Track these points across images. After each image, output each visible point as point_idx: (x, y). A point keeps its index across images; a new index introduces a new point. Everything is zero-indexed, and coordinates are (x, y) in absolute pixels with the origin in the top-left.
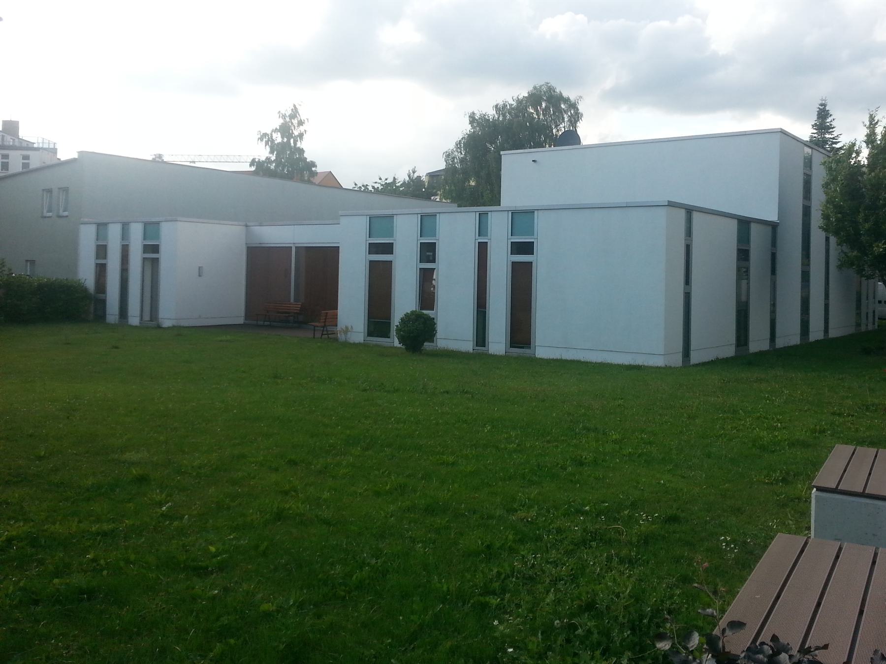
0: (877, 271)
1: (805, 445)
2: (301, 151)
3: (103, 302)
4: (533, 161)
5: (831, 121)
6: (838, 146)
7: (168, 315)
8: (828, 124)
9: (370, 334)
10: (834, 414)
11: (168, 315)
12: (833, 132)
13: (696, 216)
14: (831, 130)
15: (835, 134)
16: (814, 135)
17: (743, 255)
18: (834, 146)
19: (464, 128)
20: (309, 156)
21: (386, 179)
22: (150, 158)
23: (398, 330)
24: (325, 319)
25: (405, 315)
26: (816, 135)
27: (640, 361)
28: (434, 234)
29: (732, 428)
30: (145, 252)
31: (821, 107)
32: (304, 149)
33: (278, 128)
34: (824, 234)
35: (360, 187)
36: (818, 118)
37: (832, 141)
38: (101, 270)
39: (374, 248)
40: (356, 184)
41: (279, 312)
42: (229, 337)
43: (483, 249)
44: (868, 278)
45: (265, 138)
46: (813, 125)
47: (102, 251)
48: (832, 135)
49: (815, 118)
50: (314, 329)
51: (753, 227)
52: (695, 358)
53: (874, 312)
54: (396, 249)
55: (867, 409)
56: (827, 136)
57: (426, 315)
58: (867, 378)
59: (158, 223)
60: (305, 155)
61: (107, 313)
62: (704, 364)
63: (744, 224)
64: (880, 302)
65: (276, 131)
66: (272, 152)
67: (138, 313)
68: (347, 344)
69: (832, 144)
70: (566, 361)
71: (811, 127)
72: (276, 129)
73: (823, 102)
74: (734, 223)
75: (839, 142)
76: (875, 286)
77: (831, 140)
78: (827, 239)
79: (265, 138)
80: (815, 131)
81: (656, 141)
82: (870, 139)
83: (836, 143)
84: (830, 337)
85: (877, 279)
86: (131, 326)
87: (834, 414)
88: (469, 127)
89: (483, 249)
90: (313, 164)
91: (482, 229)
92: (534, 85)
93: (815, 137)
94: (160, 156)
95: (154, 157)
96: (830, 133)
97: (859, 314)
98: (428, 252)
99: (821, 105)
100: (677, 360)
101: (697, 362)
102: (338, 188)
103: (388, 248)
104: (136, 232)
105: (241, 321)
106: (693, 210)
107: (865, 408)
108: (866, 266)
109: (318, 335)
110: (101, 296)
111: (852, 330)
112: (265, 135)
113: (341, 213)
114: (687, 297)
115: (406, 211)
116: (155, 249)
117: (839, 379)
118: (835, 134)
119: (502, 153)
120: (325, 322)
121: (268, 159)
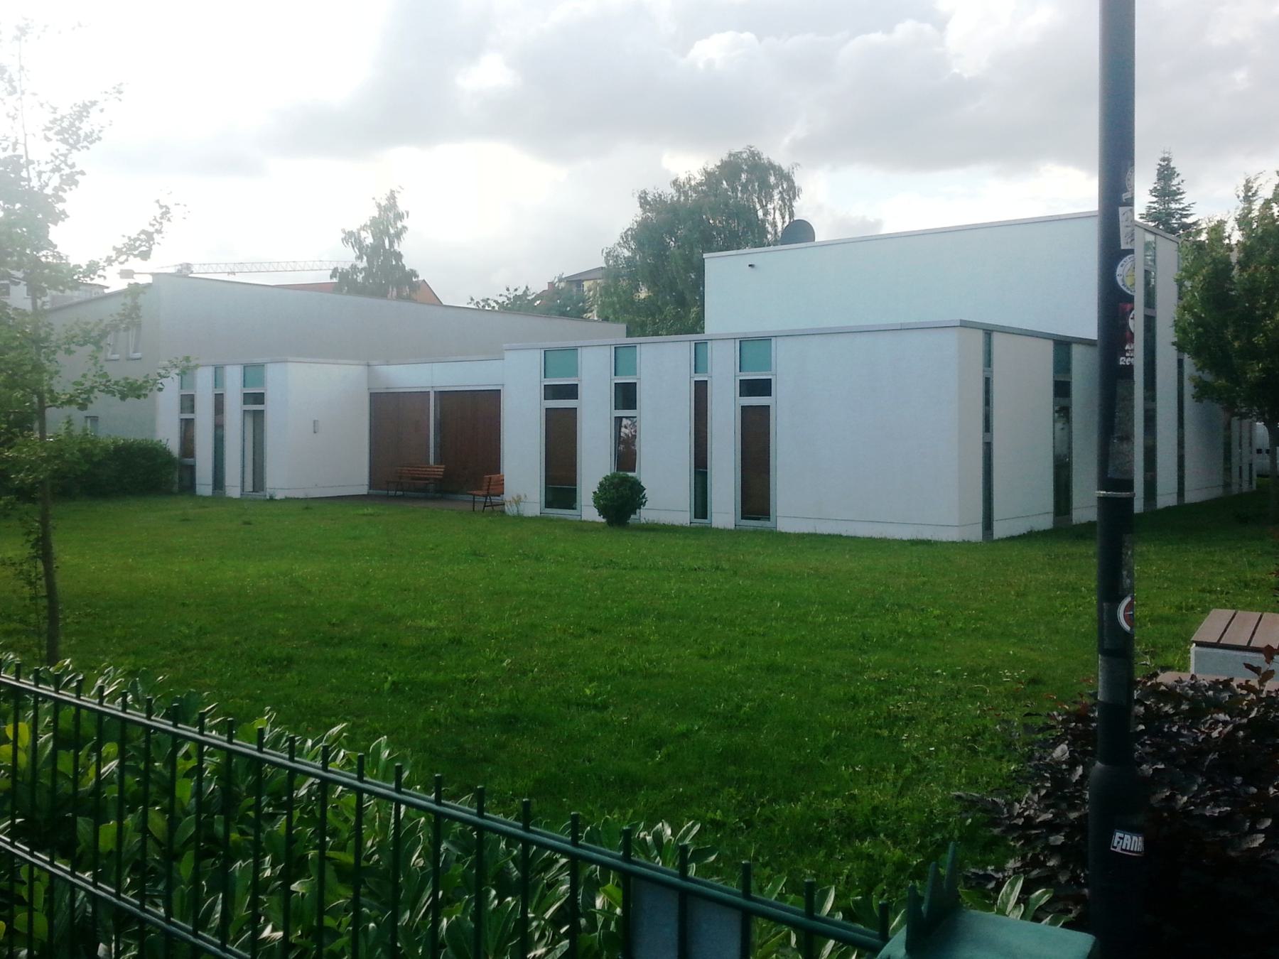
0: (1255, 408)
1: (1167, 620)
2: (399, 256)
3: (192, 468)
4: (750, 265)
5: (1179, 184)
6: (1189, 220)
7: (279, 482)
8: (1175, 188)
9: (549, 504)
10: (1203, 591)
11: (279, 482)
12: (1181, 199)
13: (997, 338)
14: (1179, 197)
15: (1185, 202)
16: (1152, 205)
17: (1062, 389)
18: (1184, 220)
19: (629, 215)
20: (408, 263)
21: (516, 290)
22: (172, 270)
23: (597, 499)
24: (489, 486)
25: (605, 478)
26: (1156, 205)
27: (927, 534)
28: (633, 370)
29: (1075, 605)
30: (245, 403)
31: (1163, 163)
32: (402, 253)
33: (369, 223)
34: (1176, 352)
35: (478, 303)
36: (1159, 179)
37: (1181, 214)
38: (187, 427)
39: (553, 392)
40: (472, 299)
41: (413, 479)
42: (370, 511)
43: (701, 390)
44: (1243, 416)
45: (351, 238)
46: (1151, 191)
47: (188, 403)
48: (1180, 204)
49: (1155, 179)
50: (474, 501)
51: (1076, 350)
52: (1000, 531)
53: (1251, 465)
54: (582, 391)
55: (1246, 586)
56: (1173, 206)
57: (632, 477)
58: (1244, 550)
59: (262, 365)
60: (404, 261)
61: (197, 482)
62: (1012, 538)
63: (1063, 345)
64: (1259, 451)
65: (364, 228)
66: (360, 258)
67: (238, 482)
68: (520, 519)
69: (1180, 219)
70: (822, 535)
71: (1149, 192)
72: (365, 225)
73: (1166, 155)
74: (1049, 346)
75: (1191, 214)
76: (1251, 429)
77: (1180, 212)
78: (1180, 363)
79: (351, 238)
80: (1155, 199)
81: (921, 233)
82: (1243, 221)
83: (1186, 216)
84: (1186, 502)
85: (1255, 419)
86: (231, 499)
87: (1203, 591)
88: (639, 211)
89: (701, 390)
90: (413, 273)
91: (699, 363)
92: (727, 152)
93: (1155, 208)
94: (188, 266)
95: (180, 267)
96: (1177, 201)
97: (1228, 470)
98: (626, 396)
99: (1164, 160)
100: (976, 534)
101: (1020, 528)
102: (434, 305)
103: (571, 391)
104: (233, 377)
105: (364, 490)
106: (993, 331)
107: (1242, 584)
108: (1238, 401)
109: (479, 507)
110: (188, 461)
111: (1218, 492)
112: (351, 234)
113: (506, 346)
114: (988, 447)
115: (595, 342)
116: (259, 398)
117: (1206, 553)
118: (1185, 202)
119: (705, 256)
120: (488, 490)
121: (354, 267)
